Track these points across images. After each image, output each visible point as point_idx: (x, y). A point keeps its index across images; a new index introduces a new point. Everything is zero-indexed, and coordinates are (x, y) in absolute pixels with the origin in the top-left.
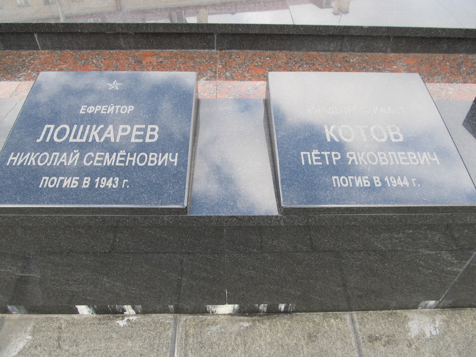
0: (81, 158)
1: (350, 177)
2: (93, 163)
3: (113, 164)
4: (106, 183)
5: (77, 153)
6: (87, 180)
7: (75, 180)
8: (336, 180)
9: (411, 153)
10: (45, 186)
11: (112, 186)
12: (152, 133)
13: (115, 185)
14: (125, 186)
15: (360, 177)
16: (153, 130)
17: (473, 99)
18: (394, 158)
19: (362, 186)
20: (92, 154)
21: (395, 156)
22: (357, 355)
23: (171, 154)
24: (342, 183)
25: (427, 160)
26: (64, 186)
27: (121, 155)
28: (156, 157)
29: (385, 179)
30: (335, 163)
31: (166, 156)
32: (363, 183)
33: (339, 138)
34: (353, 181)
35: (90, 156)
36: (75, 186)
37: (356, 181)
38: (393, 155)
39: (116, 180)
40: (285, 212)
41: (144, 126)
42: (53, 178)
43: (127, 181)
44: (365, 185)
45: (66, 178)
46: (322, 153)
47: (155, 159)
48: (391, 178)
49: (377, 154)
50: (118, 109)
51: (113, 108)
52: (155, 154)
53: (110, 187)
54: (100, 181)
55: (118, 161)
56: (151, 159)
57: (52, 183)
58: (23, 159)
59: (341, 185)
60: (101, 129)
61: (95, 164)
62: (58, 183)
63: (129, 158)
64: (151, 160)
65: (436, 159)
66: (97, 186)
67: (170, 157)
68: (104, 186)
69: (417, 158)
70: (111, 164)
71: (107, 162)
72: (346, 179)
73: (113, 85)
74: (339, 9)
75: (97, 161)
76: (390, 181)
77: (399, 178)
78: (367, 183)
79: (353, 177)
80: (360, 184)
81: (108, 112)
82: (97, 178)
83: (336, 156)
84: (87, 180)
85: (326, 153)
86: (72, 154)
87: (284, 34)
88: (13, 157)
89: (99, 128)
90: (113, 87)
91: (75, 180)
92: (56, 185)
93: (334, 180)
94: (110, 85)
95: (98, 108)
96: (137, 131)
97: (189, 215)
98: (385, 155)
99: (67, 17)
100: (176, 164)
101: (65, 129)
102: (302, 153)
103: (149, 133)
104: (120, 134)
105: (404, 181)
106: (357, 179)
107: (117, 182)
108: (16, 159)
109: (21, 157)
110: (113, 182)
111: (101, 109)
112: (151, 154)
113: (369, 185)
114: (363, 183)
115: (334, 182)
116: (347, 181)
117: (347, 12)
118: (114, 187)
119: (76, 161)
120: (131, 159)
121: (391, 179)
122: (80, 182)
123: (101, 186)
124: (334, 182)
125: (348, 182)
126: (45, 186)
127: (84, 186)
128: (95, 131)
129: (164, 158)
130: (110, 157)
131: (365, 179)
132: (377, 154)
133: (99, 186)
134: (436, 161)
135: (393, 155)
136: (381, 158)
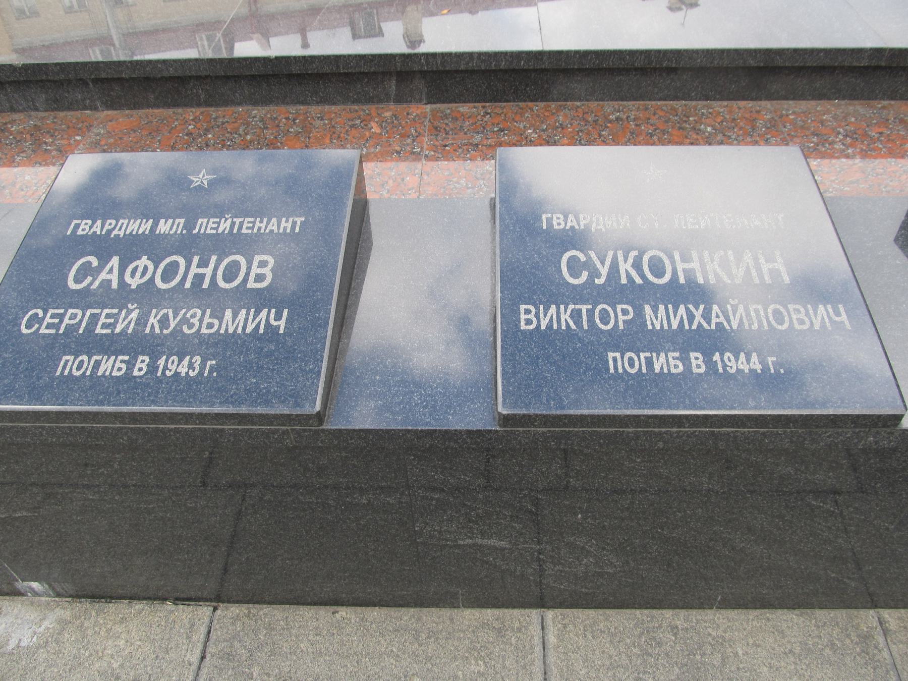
1: (642, 355)
2: (39, 329)
3: (240, 331)
5: (133, 310)
7: (122, 361)
8: (615, 360)
9: (625, 306)
10: (66, 373)
11: (187, 373)
13: (194, 371)
14: (210, 372)
15: (663, 355)
16: (263, 264)
18: (758, 315)
19: (666, 371)
20: (40, 312)
21: (762, 313)
22: (191, 678)
23: (273, 311)
24: (626, 365)
25: (827, 320)
27: (260, 262)
29: (715, 359)
32: (668, 365)
33: (705, 278)
34: (649, 362)
38: (757, 311)
39: (196, 362)
42: (80, 358)
43: (214, 362)
44: (673, 371)
45: (106, 357)
50: (238, 223)
51: (229, 222)
53: (183, 374)
54: (167, 361)
56: (255, 270)
59: (623, 367)
61: (43, 331)
62: (90, 369)
65: (844, 317)
66: (159, 374)
68: (172, 373)
69: (807, 314)
70: (235, 331)
72: (636, 358)
73: (199, 178)
75: (48, 324)
76: (722, 361)
77: (742, 356)
78: (676, 366)
79: (648, 354)
80: (662, 368)
81: (220, 231)
83: (625, 312)
84: (143, 361)
85: (584, 308)
86: (124, 312)
91: (122, 361)
92: (84, 373)
93: (611, 362)
94: (194, 179)
95: (110, 224)
98: (802, 310)
100: (281, 331)
101: (175, 265)
105: (740, 362)
106: (658, 359)
107: (197, 366)
110: (191, 366)
111: (247, 225)
112: (619, 307)
114: (668, 365)
116: (626, 365)
118: (192, 374)
119: (132, 324)
121: (726, 358)
122: (130, 365)
123: (168, 373)
124: (60, 369)
126: (66, 373)
127: (136, 373)
128: (625, 262)
129: (258, 320)
130: (235, 316)
131: (674, 358)
133: (163, 373)
135: (757, 311)
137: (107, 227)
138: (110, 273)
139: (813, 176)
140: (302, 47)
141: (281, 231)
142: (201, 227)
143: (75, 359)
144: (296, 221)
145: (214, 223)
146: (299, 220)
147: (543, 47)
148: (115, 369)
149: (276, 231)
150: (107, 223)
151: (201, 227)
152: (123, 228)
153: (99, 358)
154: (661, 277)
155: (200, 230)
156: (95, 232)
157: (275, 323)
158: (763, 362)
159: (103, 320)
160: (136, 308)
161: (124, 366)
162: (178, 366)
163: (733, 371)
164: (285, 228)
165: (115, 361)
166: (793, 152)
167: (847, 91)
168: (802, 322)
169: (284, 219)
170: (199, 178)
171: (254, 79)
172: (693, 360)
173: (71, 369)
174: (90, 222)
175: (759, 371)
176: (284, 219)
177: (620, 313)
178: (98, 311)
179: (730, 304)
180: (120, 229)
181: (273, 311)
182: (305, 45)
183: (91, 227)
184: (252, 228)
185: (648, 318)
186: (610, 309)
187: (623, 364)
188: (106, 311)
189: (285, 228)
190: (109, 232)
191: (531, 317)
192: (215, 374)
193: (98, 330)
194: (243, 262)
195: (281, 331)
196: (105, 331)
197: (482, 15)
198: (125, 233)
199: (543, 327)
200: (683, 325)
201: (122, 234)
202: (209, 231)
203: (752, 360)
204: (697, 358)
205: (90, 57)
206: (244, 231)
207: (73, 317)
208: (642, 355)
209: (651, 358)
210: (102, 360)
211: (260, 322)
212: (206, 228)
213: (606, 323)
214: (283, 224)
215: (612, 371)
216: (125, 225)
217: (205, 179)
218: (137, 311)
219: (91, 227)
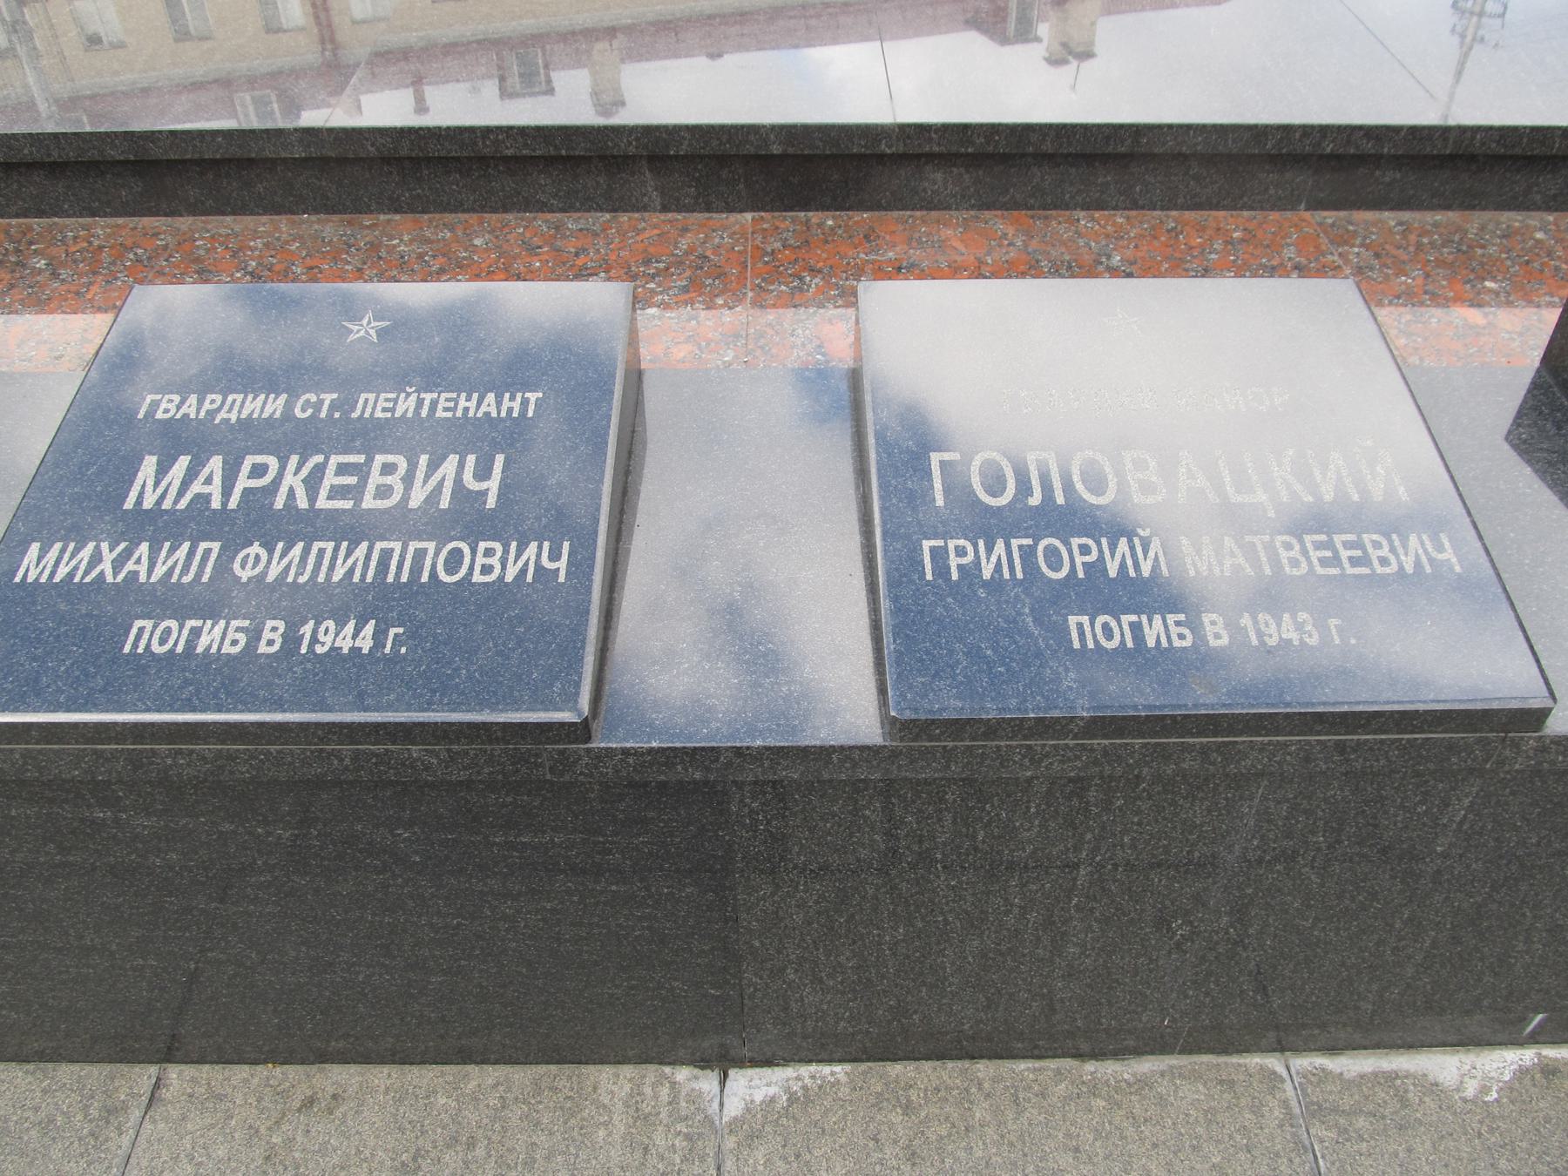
1: (1127, 619)
6: (274, 629)
7: (238, 630)
8: (1080, 626)
9: (1084, 540)
15: (1157, 619)
25: (1424, 559)
26: (199, 650)
28: (499, 554)
30: (955, 576)
31: (533, 548)
32: (1169, 637)
34: (1136, 628)
35: (308, 401)
41: (361, 459)
43: (401, 630)
44: (1177, 643)
47: (495, 561)
49: (1067, 544)
50: (427, 403)
52: (498, 546)
53: (365, 651)
54: (315, 632)
56: (480, 560)
58: (74, 563)
59: (1096, 641)
60: (317, 466)
64: (483, 566)
67: (545, 554)
68: (326, 648)
69: (1393, 550)
71: (27, 570)
72: (1113, 624)
73: (362, 325)
74: (1064, 45)
78: (1181, 637)
79: (1134, 618)
82: (304, 622)
83: (1085, 550)
89: (310, 465)
90: (362, 333)
91: (238, 630)
95: (213, 401)
96: (337, 474)
98: (1385, 543)
99: (73, 102)
102: (927, 544)
103: (375, 479)
104: (243, 482)
110: (1299, 627)
112: (482, 545)
113: (1187, 643)
114: (1169, 637)
115: (1074, 635)
116: (1116, 630)
117: (1087, 55)
122: (255, 635)
124: (1074, 635)
125: (1119, 636)
127: (263, 648)
129: (520, 564)
131: (1178, 624)
137: (207, 406)
138: (210, 485)
140: (415, 112)
141: (503, 414)
143: (155, 627)
144: (424, 399)
145: (387, 400)
146: (328, 398)
148: (227, 642)
149: (494, 415)
150: (208, 401)
152: (236, 408)
154: (1103, 493)
155: (363, 412)
156: (487, 414)
161: (242, 638)
162: (337, 635)
164: (510, 410)
165: (226, 629)
167: (315, 199)
168: (1294, 563)
169: (507, 395)
171: (977, 160)
174: (177, 398)
176: (507, 395)
177: (1076, 551)
179: (1137, 535)
181: (546, 544)
182: (421, 107)
183: (178, 408)
184: (454, 409)
185: (26, 562)
189: (510, 410)
190: (212, 414)
191: (1385, 552)
195: (562, 579)
197: (730, 60)
198: (238, 418)
199: (509, 578)
200: (287, 574)
201: (233, 417)
202: (379, 414)
203: (362, 635)
204: (1213, 623)
205: (274, 120)
206: (440, 414)
209: (1140, 623)
210: (202, 628)
211: (176, 562)
212: (374, 408)
213: (1055, 567)
214: (506, 403)
216: (371, 403)
217: (373, 328)
219: (178, 408)
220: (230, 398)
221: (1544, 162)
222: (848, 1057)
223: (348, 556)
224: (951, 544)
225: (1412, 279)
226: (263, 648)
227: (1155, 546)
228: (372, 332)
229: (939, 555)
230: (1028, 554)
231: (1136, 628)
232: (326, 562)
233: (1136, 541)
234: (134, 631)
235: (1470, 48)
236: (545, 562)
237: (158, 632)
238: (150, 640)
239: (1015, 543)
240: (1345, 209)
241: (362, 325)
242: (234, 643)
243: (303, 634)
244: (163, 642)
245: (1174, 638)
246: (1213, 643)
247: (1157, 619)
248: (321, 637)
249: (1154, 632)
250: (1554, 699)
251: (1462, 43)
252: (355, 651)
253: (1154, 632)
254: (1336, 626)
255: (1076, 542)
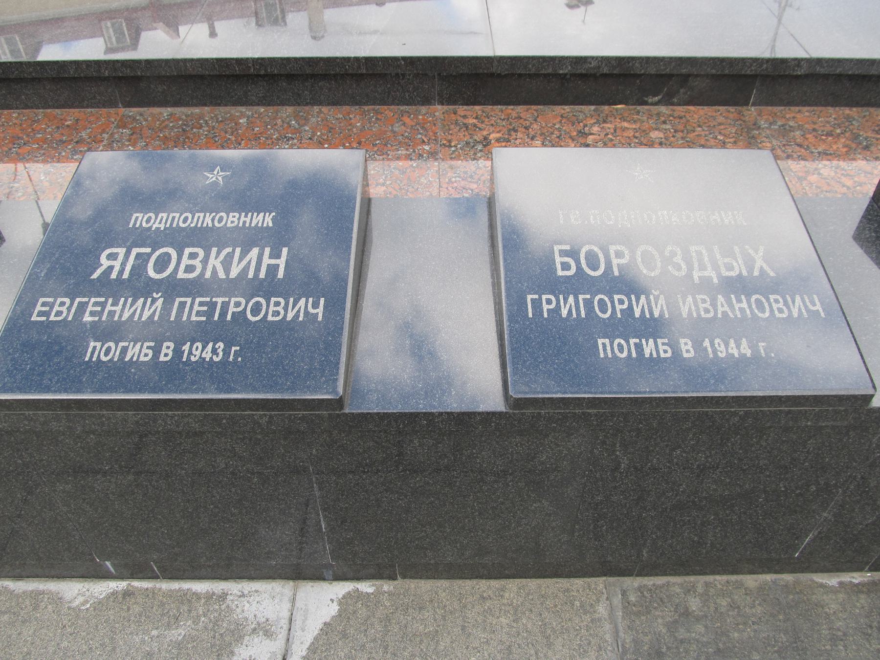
0: (167, 308)
1: (632, 341)
4: (201, 353)
7: (148, 348)
8: (604, 345)
11: (211, 358)
12: (191, 262)
14: (235, 359)
15: (651, 341)
17: (871, 190)
19: (655, 355)
23: (311, 300)
28: (283, 304)
29: (184, 348)
30: (546, 315)
31: (302, 301)
34: (639, 347)
36: (147, 359)
37: (645, 346)
39: (219, 347)
40: (519, 404)
43: (238, 348)
44: (663, 355)
45: (132, 344)
46: (214, 300)
48: (717, 341)
49: (768, 300)
53: (207, 359)
55: (194, 313)
57: (107, 353)
62: (118, 353)
63: (109, 308)
67: (310, 305)
68: (197, 358)
75: (91, 312)
78: (665, 352)
82: (185, 344)
83: (621, 302)
84: (168, 348)
86: (150, 300)
87: (725, 75)
88: (112, 305)
90: (214, 179)
91: (148, 348)
92: (113, 357)
93: (601, 347)
94: (208, 175)
97: (347, 411)
98: (781, 300)
100: (320, 318)
102: (529, 297)
108: (118, 309)
109: (128, 305)
110: (214, 351)
112: (273, 300)
113: (669, 355)
118: (216, 359)
120: (273, 262)
122: (157, 351)
123: (193, 359)
124: (88, 355)
125: (627, 350)
127: (162, 358)
128: (216, 258)
131: (663, 344)
132: (768, 300)
134: (818, 310)
136: (775, 306)
139: (784, 178)
142: (198, 220)
147: (494, 53)
148: (142, 354)
151: (198, 220)
152: (164, 221)
153: (125, 344)
157: (315, 311)
158: (753, 346)
159: (90, 308)
160: (161, 297)
161: (150, 353)
163: (722, 355)
164: (245, 222)
166: (765, 155)
168: (780, 311)
170: (217, 178)
172: (682, 346)
173: (99, 356)
175: (749, 355)
177: (616, 302)
178: (85, 300)
179: (652, 294)
180: (160, 223)
181: (311, 300)
186: (606, 299)
187: (115, 351)
188: (93, 300)
189: (245, 222)
192: (240, 359)
193: (34, 318)
194: (174, 255)
196: (39, 319)
199: (289, 318)
201: (162, 227)
207: (237, 304)
208: (632, 341)
211: (156, 310)
214: (243, 219)
215: (602, 355)
217: (220, 176)
218: (162, 300)
220: (160, 215)
221: (246, 78)
222: (145, 577)
223: (131, 306)
224: (544, 297)
225: (839, 146)
226: (162, 358)
227: (661, 301)
228: (220, 178)
229: (537, 304)
230: (589, 304)
231: (639, 347)
232: (187, 310)
233: (651, 297)
234: (90, 350)
235: (784, 10)
236: (311, 310)
237: (104, 349)
238: (100, 352)
239: (581, 297)
240: (145, 107)
241: (214, 174)
242: (146, 355)
243: (184, 350)
244: (106, 354)
245: (661, 352)
246: (685, 355)
247: (651, 341)
248: (194, 352)
249: (649, 348)
250: (874, 387)
251: (780, 6)
252: (224, 362)
253: (649, 348)
254: (763, 346)
255: (616, 297)
